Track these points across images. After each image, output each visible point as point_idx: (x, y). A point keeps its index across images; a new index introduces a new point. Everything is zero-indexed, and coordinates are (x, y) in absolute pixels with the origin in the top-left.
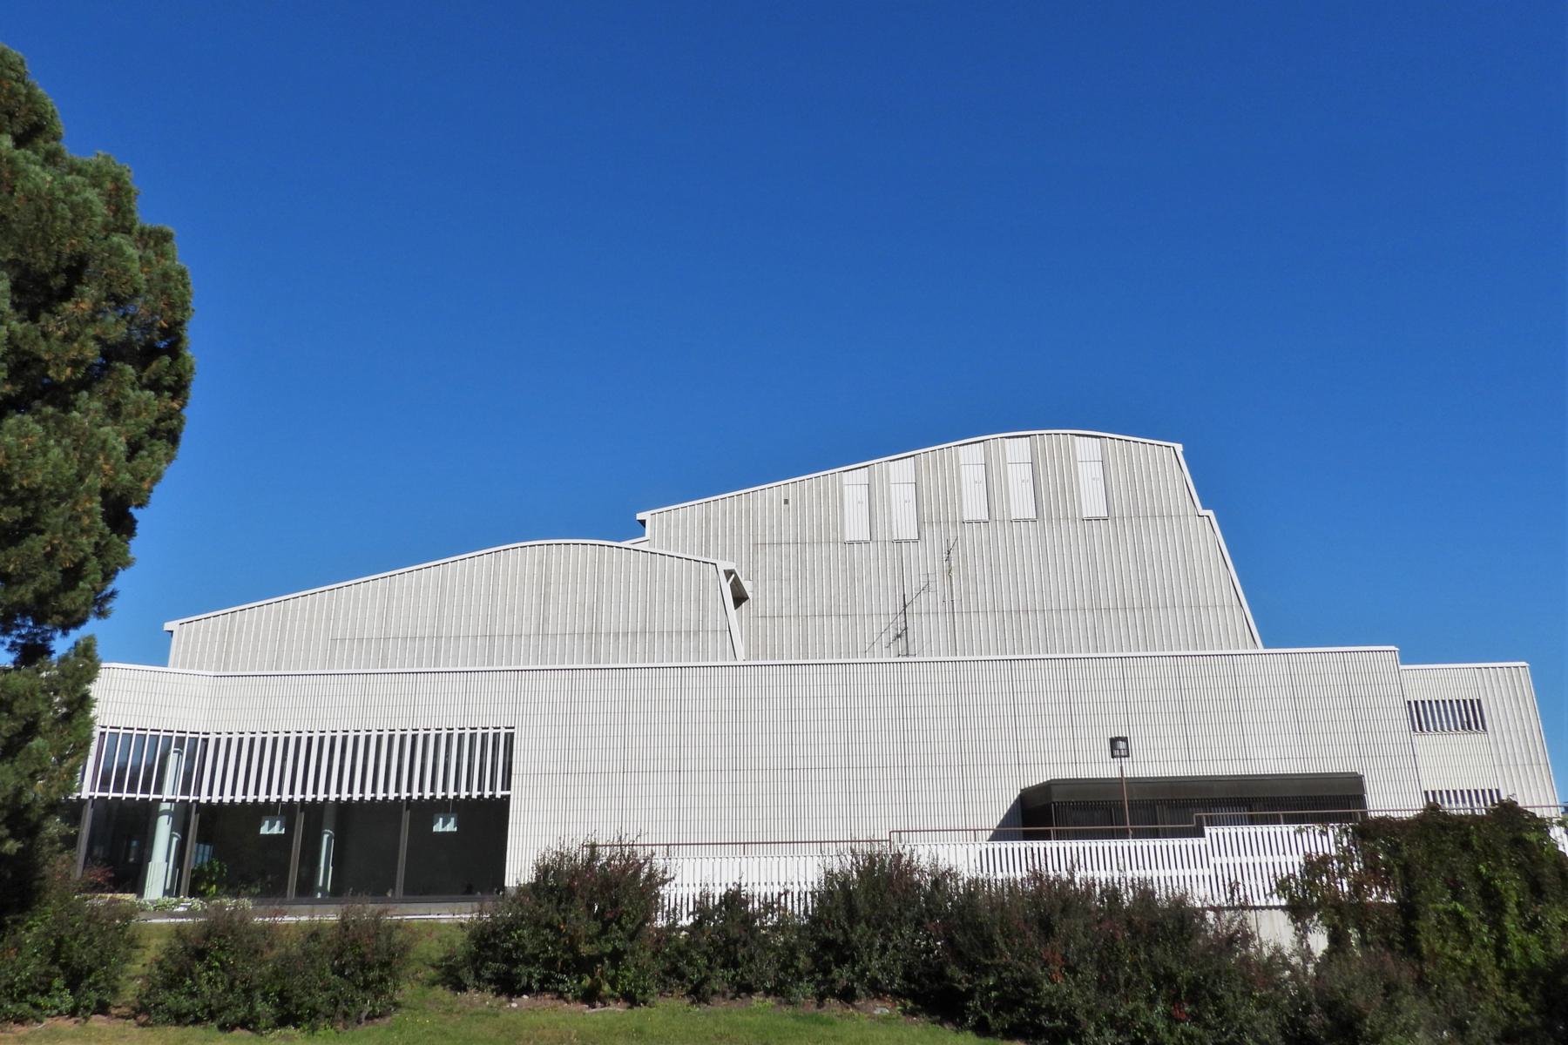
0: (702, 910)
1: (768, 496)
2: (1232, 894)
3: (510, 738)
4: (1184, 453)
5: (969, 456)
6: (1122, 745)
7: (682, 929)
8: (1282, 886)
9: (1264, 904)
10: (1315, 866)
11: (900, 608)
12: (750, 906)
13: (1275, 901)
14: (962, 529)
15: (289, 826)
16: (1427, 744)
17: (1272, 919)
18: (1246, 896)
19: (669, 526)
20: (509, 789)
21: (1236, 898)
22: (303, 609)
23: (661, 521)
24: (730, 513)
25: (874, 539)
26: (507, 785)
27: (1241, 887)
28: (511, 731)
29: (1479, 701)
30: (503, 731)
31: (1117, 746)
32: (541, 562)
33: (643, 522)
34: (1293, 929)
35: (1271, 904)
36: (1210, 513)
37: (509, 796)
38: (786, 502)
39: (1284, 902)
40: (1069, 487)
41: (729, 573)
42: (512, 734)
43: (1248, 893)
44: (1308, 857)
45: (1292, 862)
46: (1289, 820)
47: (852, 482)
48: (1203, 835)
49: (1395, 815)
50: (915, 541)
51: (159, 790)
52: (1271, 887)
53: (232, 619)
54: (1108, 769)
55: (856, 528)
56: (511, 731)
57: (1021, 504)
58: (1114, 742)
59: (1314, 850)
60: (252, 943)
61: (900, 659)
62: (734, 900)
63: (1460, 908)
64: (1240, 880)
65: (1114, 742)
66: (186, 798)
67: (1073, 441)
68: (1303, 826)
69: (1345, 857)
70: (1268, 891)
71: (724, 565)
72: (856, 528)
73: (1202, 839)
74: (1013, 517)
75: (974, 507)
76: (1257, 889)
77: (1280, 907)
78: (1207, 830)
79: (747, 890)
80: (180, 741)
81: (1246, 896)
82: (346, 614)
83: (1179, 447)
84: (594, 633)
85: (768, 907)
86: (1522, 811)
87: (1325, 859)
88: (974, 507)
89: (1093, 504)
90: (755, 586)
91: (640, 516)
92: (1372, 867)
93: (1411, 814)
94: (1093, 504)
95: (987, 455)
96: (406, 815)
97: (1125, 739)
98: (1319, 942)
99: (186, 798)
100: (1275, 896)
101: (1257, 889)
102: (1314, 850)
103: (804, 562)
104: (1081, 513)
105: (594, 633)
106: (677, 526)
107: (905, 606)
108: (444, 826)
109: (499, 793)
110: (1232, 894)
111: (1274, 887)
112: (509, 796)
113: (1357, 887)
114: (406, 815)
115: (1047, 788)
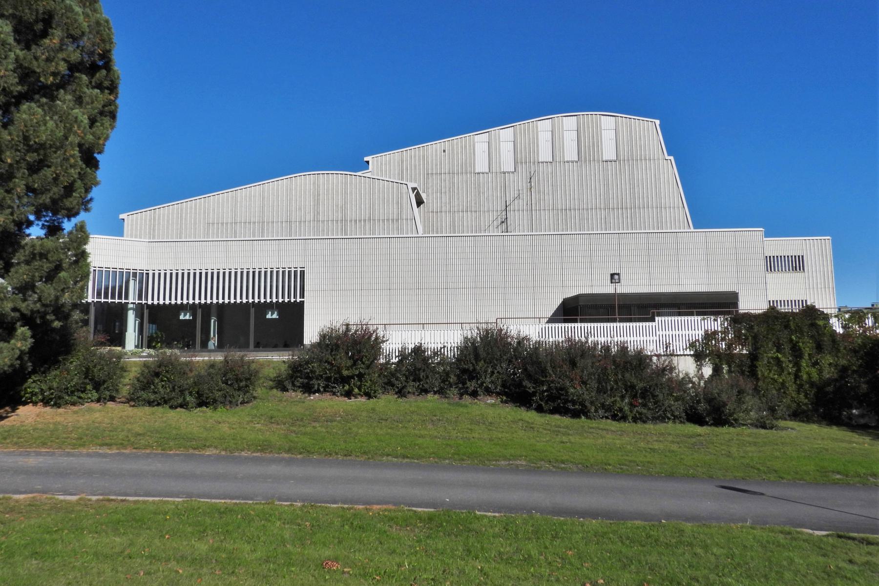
0: (403, 355)
1: (435, 147)
2: (667, 348)
3: (302, 273)
4: (660, 125)
5: (543, 126)
6: (616, 277)
7: (393, 363)
8: (692, 345)
9: (682, 353)
10: (709, 336)
11: (504, 208)
12: (426, 353)
13: (688, 352)
14: (538, 166)
15: (194, 315)
16: (772, 277)
17: (685, 360)
18: (673, 350)
19: (381, 164)
20: (303, 298)
21: (668, 350)
22: (191, 208)
23: (377, 161)
24: (414, 157)
25: (491, 171)
26: (302, 295)
27: (671, 345)
28: (303, 269)
29: (802, 256)
30: (299, 269)
31: (614, 277)
32: (314, 183)
33: (368, 162)
34: (695, 365)
35: (685, 353)
36: (672, 158)
37: (304, 301)
38: (444, 151)
39: (692, 353)
40: (597, 144)
41: (414, 189)
42: (304, 271)
43: (675, 348)
44: (706, 331)
45: (699, 334)
46: (698, 314)
47: (480, 140)
48: (654, 321)
49: (753, 312)
50: (513, 173)
51: (127, 297)
52: (686, 345)
53: (155, 213)
54: (609, 289)
55: (481, 165)
56: (303, 269)
57: (571, 154)
58: (612, 275)
59: (709, 328)
60: (184, 370)
61: (504, 234)
62: (418, 350)
63: (780, 356)
64: (671, 342)
65: (612, 275)
66: (121, 301)
67: (600, 118)
68: (705, 317)
69: (725, 332)
70: (685, 347)
71: (412, 185)
72: (481, 165)
73: (654, 323)
74: (566, 160)
75: (545, 154)
76: (679, 346)
77: (690, 355)
78: (657, 318)
79: (425, 346)
80: (135, 275)
81: (673, 350)
82: (214, 210)
83: (658, 122)
84: (344, 221)
85: (435, 354)
86: (817, 310)
87: (715, 333)
88: (545, 154)
89: (609, 152)
90: (428, 196)
91: (366, 159)
92: (738, 336)
93: (761, 312)
94: (609, 152)
95: (553, 126)
96: (252, 310)
97: (618, 274)
98: (707, 371)
99: (121, 301)
100: (688, 350)
101: (679, 346)
102: (709, 328)
103: (453, 183)
104: (602, 158)
105: (344, 221)
106: (386, 164)
107: (506, 207)
108: (272, 315)
109: (298, 300)
110: (667, 348)
111: (688, 345)
112: (304, 301)
113: (729, 346)
114: (252, 310)
115: (576, 298)
